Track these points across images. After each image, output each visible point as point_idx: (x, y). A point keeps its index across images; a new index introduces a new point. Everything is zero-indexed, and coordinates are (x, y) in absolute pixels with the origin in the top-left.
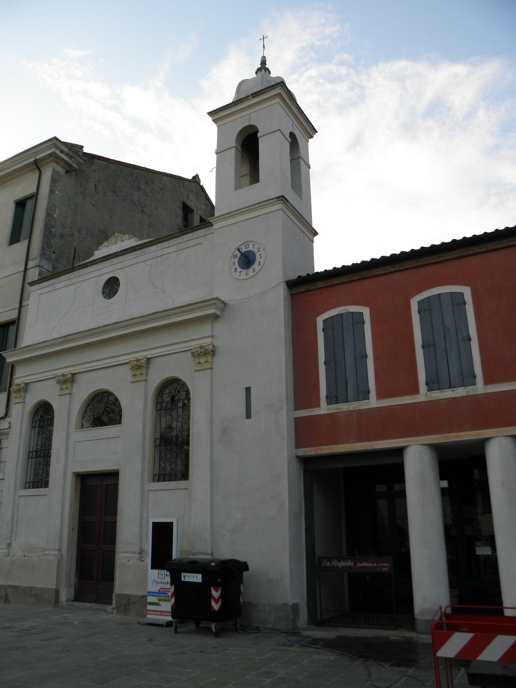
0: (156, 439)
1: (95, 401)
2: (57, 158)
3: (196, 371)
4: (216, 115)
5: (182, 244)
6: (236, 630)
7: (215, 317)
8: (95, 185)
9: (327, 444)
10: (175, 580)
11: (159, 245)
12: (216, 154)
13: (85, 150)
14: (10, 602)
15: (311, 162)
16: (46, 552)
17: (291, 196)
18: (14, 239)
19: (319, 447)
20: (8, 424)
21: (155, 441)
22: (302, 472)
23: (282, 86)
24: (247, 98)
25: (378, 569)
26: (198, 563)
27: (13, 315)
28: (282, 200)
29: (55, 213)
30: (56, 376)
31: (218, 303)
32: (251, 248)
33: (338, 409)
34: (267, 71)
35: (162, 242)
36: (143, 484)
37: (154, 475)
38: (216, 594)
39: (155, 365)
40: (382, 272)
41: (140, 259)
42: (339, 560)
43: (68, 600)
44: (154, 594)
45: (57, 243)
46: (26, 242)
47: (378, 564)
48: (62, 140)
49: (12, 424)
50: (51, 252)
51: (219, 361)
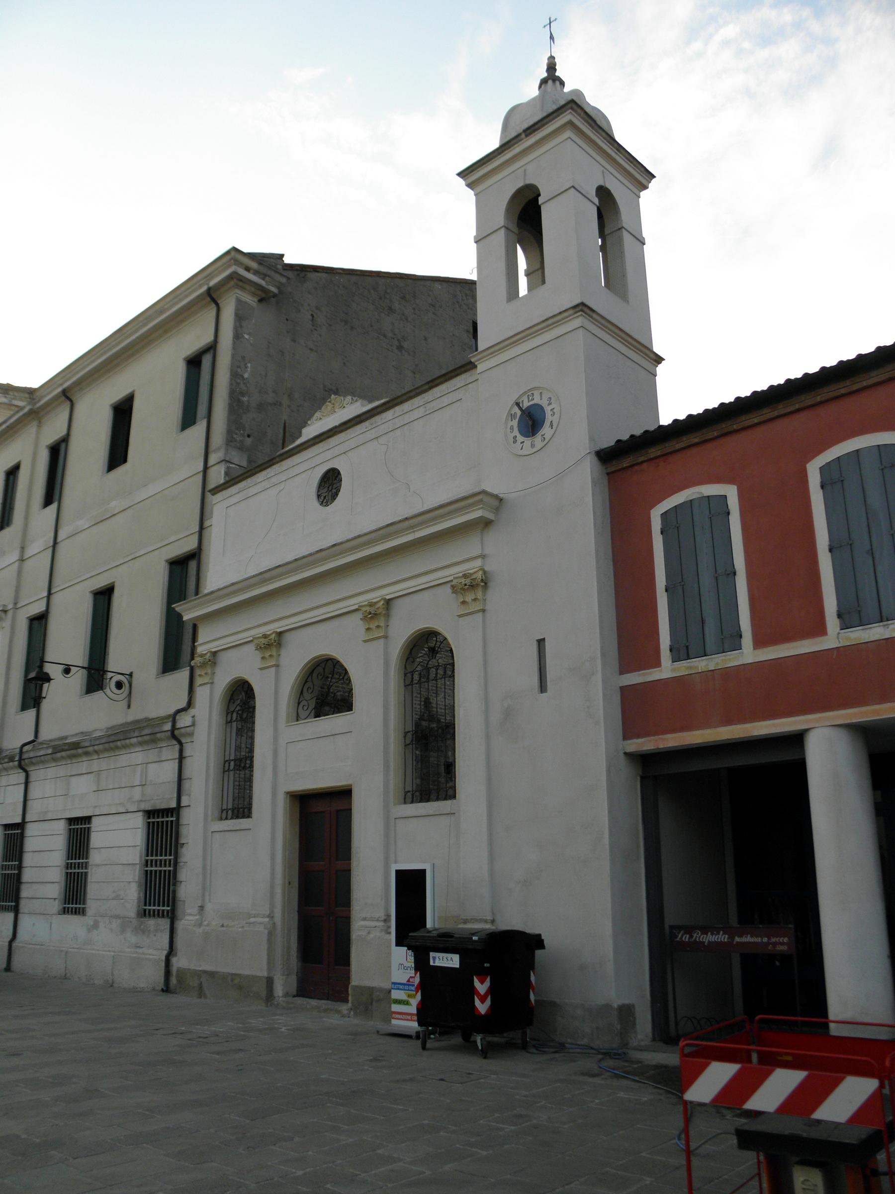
0: (406, 733)
1: (315, 675)
2: (241, 280)
3: (460, 616)
4: (471, 174)
5: (432, 404)
6: (524, 1047)
7: (486, 524)
8: (312, 315)
9: (674, 730)
10: (421, 964)
11: (397, 409)
12: (476, 242)
13: (287, 260)
14: (205, 997)
15: (647, 232)
16: (252, 920)
17: (603, 302)
18: (188, 420)
19: (661, 736)
20: (191, 719)
21: (405, 737)
22: (639, 778)
23: (572, 108)
24: (516, 139)
25: (770, 947)
26: (452, 937)
27: (191, 545)
28: (582, 311)
29: (246, 371)
30: (255, 638)
31: (486, 499)
32: (537, 400)
33: (691, 668)
34: (558, 83)
35: (401, 403)
36: (386, 807)
37: (406, 793)
38: (481, 987)
39: (400, 610)
40: (756, 421)
41: (371, 434)
42: (705, 930)
43: (286, 995)
44: (401, 987)
45: (254, 419)
46: (204, 423)
47: (769, 939)
48: (245, 250)
49: (196, 718)
50: (243, 436)
51: (495, 598)
